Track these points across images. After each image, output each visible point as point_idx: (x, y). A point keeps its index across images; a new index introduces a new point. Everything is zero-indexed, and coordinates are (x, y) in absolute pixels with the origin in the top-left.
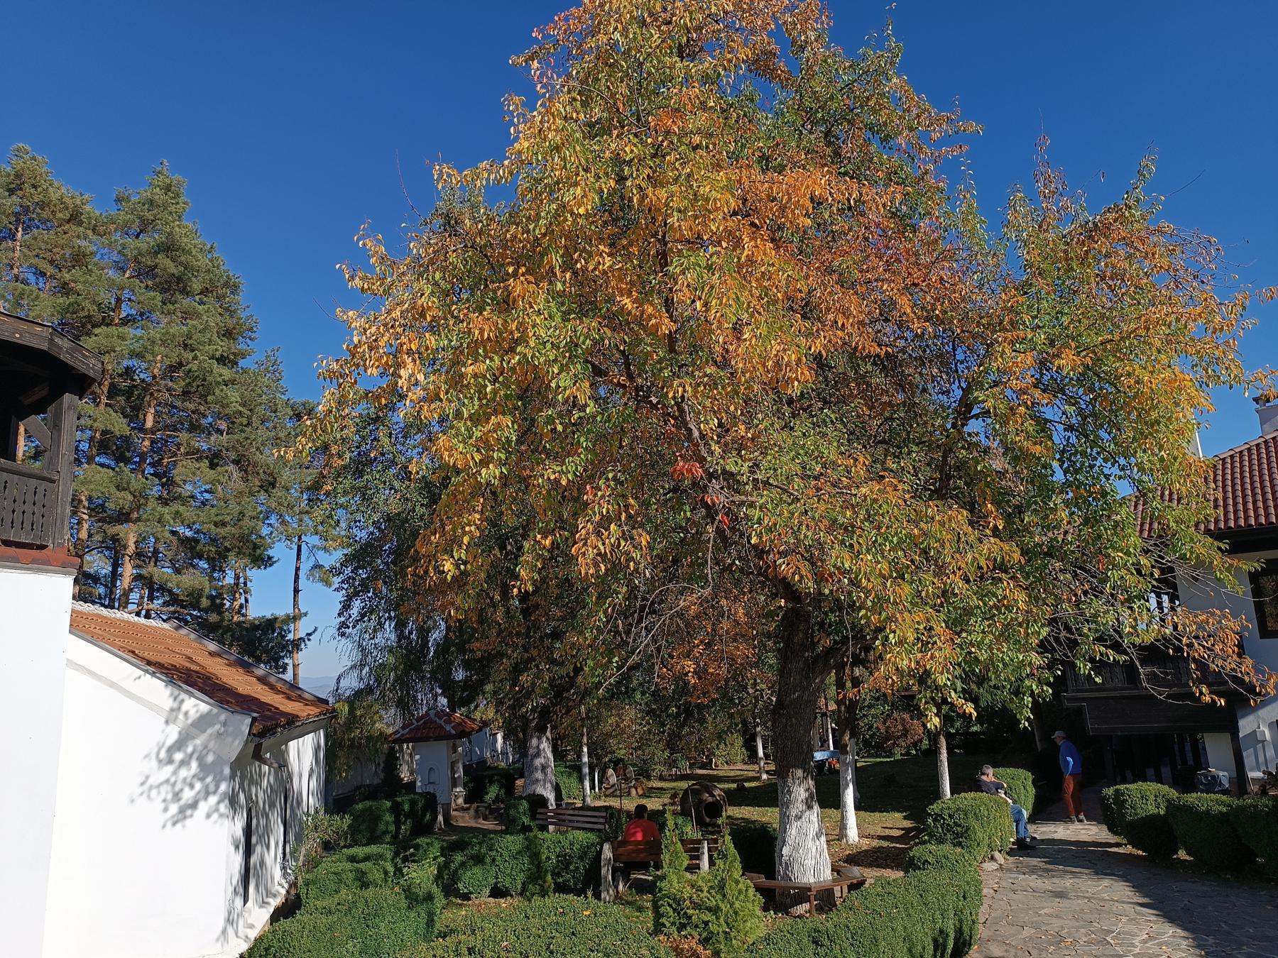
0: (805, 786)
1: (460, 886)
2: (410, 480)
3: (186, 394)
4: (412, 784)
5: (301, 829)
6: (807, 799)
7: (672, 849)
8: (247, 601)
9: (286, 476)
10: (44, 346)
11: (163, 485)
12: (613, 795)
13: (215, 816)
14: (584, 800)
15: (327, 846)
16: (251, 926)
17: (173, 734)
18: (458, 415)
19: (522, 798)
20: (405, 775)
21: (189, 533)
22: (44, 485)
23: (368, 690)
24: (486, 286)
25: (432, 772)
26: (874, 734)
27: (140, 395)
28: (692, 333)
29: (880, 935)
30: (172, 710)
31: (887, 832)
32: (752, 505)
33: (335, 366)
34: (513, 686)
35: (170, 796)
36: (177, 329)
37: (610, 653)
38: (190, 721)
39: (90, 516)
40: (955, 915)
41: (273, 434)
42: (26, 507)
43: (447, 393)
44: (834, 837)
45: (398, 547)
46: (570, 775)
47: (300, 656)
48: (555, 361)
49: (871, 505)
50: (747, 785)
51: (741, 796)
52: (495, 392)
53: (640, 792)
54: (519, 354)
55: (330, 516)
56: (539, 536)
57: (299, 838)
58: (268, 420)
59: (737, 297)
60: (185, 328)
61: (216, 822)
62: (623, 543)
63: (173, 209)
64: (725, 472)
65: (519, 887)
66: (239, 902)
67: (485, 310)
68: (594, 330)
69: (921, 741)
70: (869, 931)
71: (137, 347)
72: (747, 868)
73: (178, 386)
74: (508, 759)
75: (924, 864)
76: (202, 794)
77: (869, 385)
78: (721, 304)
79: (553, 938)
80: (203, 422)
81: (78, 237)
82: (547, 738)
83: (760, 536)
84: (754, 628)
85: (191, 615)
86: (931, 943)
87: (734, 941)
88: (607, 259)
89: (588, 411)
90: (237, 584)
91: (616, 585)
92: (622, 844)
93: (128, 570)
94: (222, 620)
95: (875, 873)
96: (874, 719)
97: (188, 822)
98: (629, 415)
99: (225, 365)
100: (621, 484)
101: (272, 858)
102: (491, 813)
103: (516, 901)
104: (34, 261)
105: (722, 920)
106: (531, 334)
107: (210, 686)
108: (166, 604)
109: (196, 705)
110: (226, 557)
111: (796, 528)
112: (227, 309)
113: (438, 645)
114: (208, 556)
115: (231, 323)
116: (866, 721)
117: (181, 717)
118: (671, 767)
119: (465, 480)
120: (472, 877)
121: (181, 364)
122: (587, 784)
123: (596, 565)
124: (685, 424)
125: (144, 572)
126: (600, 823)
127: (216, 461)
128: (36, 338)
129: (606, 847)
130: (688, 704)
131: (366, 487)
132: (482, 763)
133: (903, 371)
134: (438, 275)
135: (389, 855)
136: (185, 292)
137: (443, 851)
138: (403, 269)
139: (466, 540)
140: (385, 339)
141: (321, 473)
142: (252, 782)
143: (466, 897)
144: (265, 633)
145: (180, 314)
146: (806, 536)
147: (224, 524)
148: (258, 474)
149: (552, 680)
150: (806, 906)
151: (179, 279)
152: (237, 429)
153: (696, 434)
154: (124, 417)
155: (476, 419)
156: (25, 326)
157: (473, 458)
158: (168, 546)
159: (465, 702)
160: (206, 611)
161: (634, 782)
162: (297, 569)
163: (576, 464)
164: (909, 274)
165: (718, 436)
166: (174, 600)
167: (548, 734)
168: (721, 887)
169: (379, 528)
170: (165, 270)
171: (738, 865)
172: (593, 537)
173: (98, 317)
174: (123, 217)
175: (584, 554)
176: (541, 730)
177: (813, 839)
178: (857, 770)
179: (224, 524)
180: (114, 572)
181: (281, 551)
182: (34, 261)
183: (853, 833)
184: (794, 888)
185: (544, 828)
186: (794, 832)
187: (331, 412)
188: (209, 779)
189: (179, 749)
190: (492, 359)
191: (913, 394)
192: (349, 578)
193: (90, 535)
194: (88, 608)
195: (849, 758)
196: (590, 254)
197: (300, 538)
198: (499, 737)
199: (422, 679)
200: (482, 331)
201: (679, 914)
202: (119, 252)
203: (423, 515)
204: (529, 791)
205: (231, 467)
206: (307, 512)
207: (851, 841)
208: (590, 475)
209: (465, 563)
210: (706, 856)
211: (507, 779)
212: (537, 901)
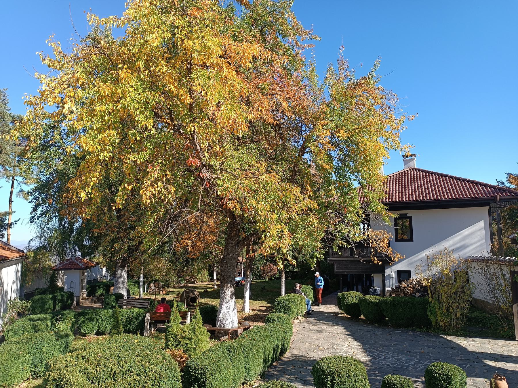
0: (231, 290)
1: (82, 331)
4: (62, 289)
6: (231, 295)
7: (175, 315)
12: (152, 294)
14: (140, 296)
18: (91, 128)
20: (60, 284)
23: (44, 247)
24: (109, 72)
25: (72, 283)
28: (199, 104)
29: (253, 348)
32: (219, 179)
37: (155, 236)
47: (11, 231)
50: (208, 290)
51: (206, 294)
52: (109, 120)
54: (121, 104)
55: (29, 169)
56: (126, 185)
59: (219, 92)
62: (163, 190)
64: (209, 165)
65: (109, 331)
69: (276, 274)
72: (205, 322)
74: (107, 278)
78: (212, 94)
79: (121, 351)
82: (125, 270)
83: (221, 192)
84: (217, 229)
86: (272, 350)
87: (197, 351)
88: (165, 67)
91: (160, 208)
96: (260, 266)
102: (98, 301)
105: (193, 343)
106: (128, 96)
111: (236, 190)
113: (78, 229)
118: (178, 283)
119: (93, 157)
120: (88, 327)
122: (142, 289)
126: (146, 305)
129: (148, 314)
132: (96, 280)
134: (86, 64)
139: (92, 184)
143: (84, 335)
149: (129, 246)
150: (227, 337)
153: (199, 148)
155: (100, 131)
157: (97, 148)
161: (162, 289)
162: (12, 192)
164: (288, 93)
167: (126, 269)
168: (194, 330)
171: (201, 321)
172: (150, 187)
176: (123, 267)
183: (247, 310)
184: (223, 330)
187: (29, 120)
190: (109, 105)
191: (285, 142)
192: (37, 197)
197: (13, 178)
198: (104, 269)
200: (105, 91)
201: (176, 341)
203: (74, 171)
209: (91, 194)
210: (189, 318)
211: (107, 287)
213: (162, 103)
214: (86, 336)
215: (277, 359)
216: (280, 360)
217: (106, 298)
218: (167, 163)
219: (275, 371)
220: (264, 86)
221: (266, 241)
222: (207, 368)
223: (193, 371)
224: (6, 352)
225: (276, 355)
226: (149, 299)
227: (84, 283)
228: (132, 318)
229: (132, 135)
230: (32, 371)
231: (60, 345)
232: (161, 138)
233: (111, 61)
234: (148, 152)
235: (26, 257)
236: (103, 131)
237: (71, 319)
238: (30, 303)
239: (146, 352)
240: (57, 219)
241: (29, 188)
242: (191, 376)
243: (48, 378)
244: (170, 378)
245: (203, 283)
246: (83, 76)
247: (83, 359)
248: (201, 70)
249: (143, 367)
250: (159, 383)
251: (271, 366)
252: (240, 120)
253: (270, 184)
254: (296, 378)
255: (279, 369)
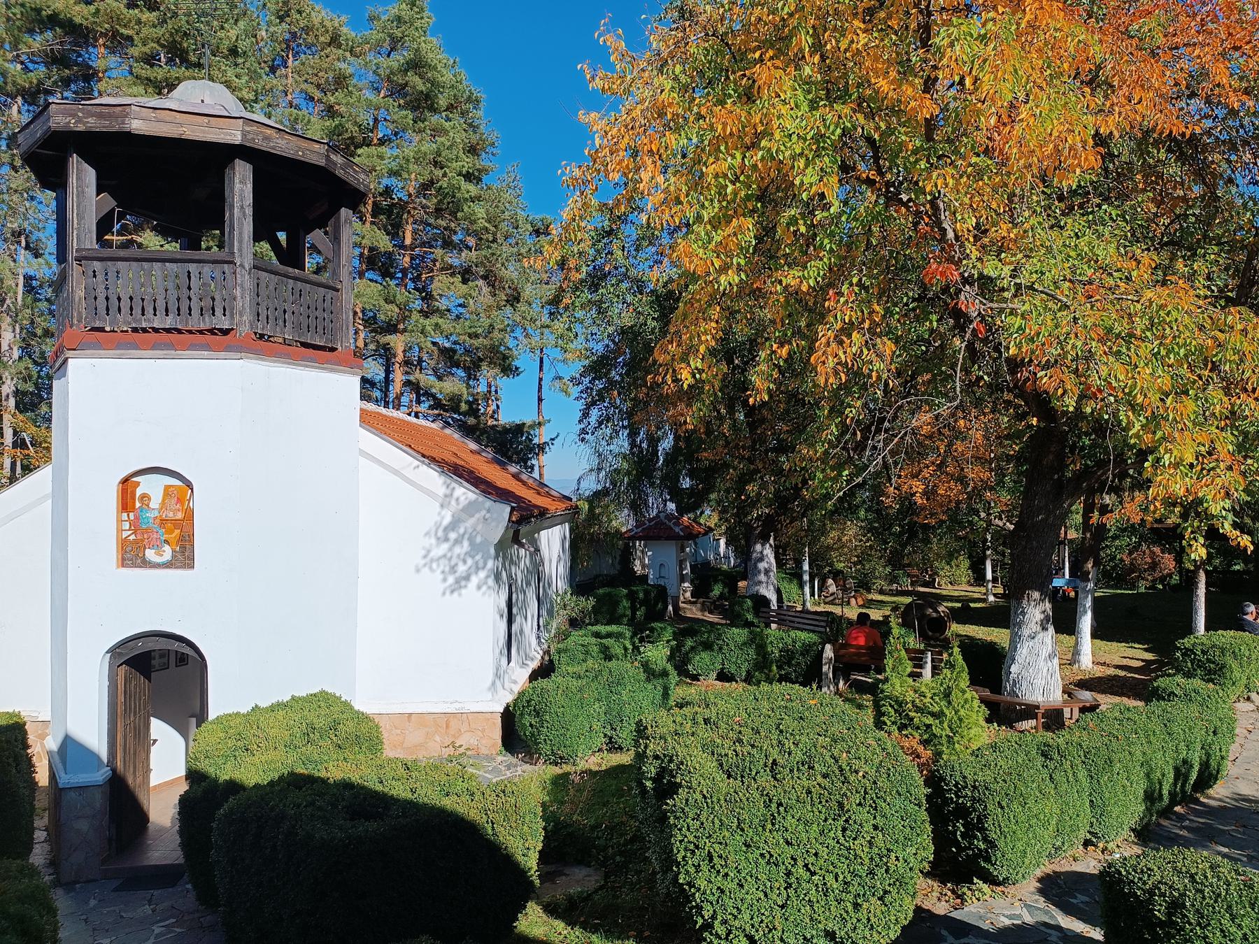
0: (1041, 607)
1: (690, 667)
2: (642, 294)
3: (438, 212)
4: (644, 578)
5: (552, 607)
6: (1042, 621)
7: (896, 655)
8: (498, 407)
9: (528, 291)
10: (322, 162)
11: (423, 299)
12: (832, 603)
13: (484, 588)
14: (804, 605)
15: (574, 623)
16: (515, 682)
17: (448, 519)
18: (699, 218)
19: (746, 597)
20: (638, 568)
21: (447, 345)
22: (330, 293)
23: (604, 493)
24: (727, 78)
26: (1116, 565)
27: (398, 213)
28: (957, 115)
29: (1115, 757)
30: (446, 496)
31: (1125, 662)
32: (1013, 312)
33: (577, 173)
34: (739, 496)
35: (447, 569)
36: (428, 147)
37: (839, 467)
38: (461, 507)
39: (365, 327)
40: (1202, 748)
41: (516, 250)
42: (317, 313)
43: (687, 196)
44: (1065, 661)
45: (633, 359)
46: (791, 581)
47: (544, 459)
48: (801, 154)
49: (1157, 312)
50: (972, 605)
51: (966, 614)
52: (735, 193)
53: (861, 602)
54: (763, 149)
55: (569, 329)
56: (775, 346)
57: (550, 613)
58: (511, 236)
59: (1016, 71)
60: (434, 145)
61: (484, 594)
62: (865, 352)
63: (418, 24)
64: (981, 276)
65: (744, 674)
66: (504, 660)
67: (726, 103)
68: (846, 117)
69: (1170, 575)
70: (1104, 751)
71: (395, 167)
72: (974, 682)
73: (432, 203)
74: (729, 562)
75: (1169, 695)
76: (473, 569)
77: (1160, 176)
78: (996, 78)
79: (782, 719)
80: (455, 238)
81: (339, 59)
82: (771, 545)
83: (1019, 346)
84: (992, 451)
85: (453, 418)
86: (1172, 771)
87: (957, 745)
88: (862, 35)
89: (832, 212)
90: (490, 392)
91: (850, 399)
92: (843, 646)
93: (398, 376)
94: (479, 423)
95: (1109, 700)
96: (1119, 550)
97: (463, 591)
98: (880, 213)
99: (470, 181)
100: (866, 289)
101: (527, 625)
102: (714, 608)
103: (742, 684)
104: (304, 86)
105: (945, 725)
106: (775, 127)
107: (474, 478)
108: (431, 407)
109: (464, 494)
110: (480, 366)
111: (1062, 338)
112: (470, 125)
113: (667, 454)
114: (464, 365)
115: (474, 138)
116: (1108, 551)
117: (453, 502)
118: (891, 582)
119: (702, 288)
120: (701, 660)
121: (432, 182)
122: (807, 589)
123: (836, 373)
124: (939, 223)
125: (412, 378)
126: (822, 627)
127: (467, 276)
128: (314, 154)
129: (828, 647)
130: (912, 525)
131: (601, 301)
132: (706, 564)
133: (1206, 158)
134: (678, 69)
135: (628, 634)
136: (434, 109)
137: (676, 636)
138: (643, 64)
139: (702, 349)
140: (626, 140)
141: (561, 286)
142: (512, 562)
143: (695, 678)
144: (515, 436)
145: (429, 132)
146: (1074, 346)
147: (476, 336)
148: (504, 288)
149: (777, 492)
150: (1033, 723)
151: (427, 96)
152: (484, 244)
153: (951, 235)
154: (388, 234)
155: (716, 223)
156: (305, 144)
157: (713, 264)
158: (431, 355)
159: (692, 508)
160: (464, 414)
161: (853, 593)
162: (541, 379)
163: (819, 269)
164: (1230, 34)
165: (975, 236)
166: (437, 404)
167: (772, 541)
168: (947, 695)
169: (613, 341)
170: (414, 87)
171: (965, 676)
172: (834, 345)
173: (360, 139)
174: (375, 36)
175: (824, 363)
176: (765, 539)
177: (1046, 659)
178: (1095, 600)
179: (476, 336)
180: (387, 378)
181: (524, 360)
182: (304, 86)
183: (1086, 660)
184: (1020, 704)
185: (768, 625)
186: (1024, 651)
187: (574, 220)
188: (478, 557)
189: (453, 530)
190: (733, 157)
191: (1215, 186)
192: (587, 388)
193: (366, 345)
194: (371, 407)
195: (1091, 585)
196: (843, 33)
197: (542, 350)
198: (722, 542)
199: (652, 485)
200: (725, 125)
201: (900, 715)
202: (374, 72)
203: (655, 328)
204: (751, 592)
205: (480, 282)
206: (548, 326)
207: (1083, 667)
208: (835, 275)
209: (701, 371)
210: (929, 666)
211: (731, 579)
212: (765, 687)
213: (860, 130)
214: (699, 680)
215: (1187, 799)
216: (1197, 801)
217: (734, 605)
218: (872, 284)
219: (1182, 828)
220: (1146, 29)
221: (1159, 478)
222: (987, 788)
223: (951, 790)
224: (560, 691)
225: (1183, 786)
226: (828, 614)
227: (686, 568)
228: (792, 652)
229: (787, 224)
230: (605, 735)
231: (652, 691)
232: (855, 219)
233: (730, 49)
234: (825, 260)
235: (576, 510)
236: (723, 223)
237: (668, 641)
238: (592, 602)
239: (837, 729)
240: (625, 434)
241: (576, 368)
242: (947, 802)
243: (645, 752)
244: (900, 795)
245: (956, 588)
246: (674, 98)
247: (706, 724)
248: (960, 21)
249: (837, 761)
250: (874, 802)
251: (1166, 812)
252: (1074, 140)
253: (1174, 314)
254: (1250, 858)
255: (1195, 825)
